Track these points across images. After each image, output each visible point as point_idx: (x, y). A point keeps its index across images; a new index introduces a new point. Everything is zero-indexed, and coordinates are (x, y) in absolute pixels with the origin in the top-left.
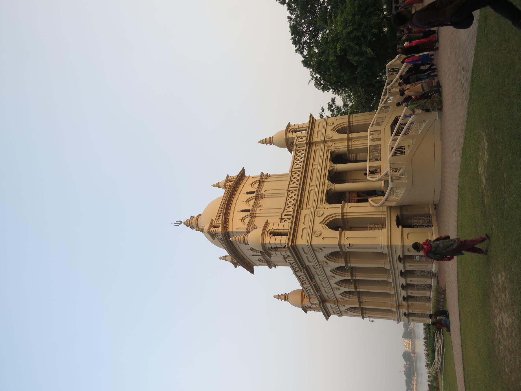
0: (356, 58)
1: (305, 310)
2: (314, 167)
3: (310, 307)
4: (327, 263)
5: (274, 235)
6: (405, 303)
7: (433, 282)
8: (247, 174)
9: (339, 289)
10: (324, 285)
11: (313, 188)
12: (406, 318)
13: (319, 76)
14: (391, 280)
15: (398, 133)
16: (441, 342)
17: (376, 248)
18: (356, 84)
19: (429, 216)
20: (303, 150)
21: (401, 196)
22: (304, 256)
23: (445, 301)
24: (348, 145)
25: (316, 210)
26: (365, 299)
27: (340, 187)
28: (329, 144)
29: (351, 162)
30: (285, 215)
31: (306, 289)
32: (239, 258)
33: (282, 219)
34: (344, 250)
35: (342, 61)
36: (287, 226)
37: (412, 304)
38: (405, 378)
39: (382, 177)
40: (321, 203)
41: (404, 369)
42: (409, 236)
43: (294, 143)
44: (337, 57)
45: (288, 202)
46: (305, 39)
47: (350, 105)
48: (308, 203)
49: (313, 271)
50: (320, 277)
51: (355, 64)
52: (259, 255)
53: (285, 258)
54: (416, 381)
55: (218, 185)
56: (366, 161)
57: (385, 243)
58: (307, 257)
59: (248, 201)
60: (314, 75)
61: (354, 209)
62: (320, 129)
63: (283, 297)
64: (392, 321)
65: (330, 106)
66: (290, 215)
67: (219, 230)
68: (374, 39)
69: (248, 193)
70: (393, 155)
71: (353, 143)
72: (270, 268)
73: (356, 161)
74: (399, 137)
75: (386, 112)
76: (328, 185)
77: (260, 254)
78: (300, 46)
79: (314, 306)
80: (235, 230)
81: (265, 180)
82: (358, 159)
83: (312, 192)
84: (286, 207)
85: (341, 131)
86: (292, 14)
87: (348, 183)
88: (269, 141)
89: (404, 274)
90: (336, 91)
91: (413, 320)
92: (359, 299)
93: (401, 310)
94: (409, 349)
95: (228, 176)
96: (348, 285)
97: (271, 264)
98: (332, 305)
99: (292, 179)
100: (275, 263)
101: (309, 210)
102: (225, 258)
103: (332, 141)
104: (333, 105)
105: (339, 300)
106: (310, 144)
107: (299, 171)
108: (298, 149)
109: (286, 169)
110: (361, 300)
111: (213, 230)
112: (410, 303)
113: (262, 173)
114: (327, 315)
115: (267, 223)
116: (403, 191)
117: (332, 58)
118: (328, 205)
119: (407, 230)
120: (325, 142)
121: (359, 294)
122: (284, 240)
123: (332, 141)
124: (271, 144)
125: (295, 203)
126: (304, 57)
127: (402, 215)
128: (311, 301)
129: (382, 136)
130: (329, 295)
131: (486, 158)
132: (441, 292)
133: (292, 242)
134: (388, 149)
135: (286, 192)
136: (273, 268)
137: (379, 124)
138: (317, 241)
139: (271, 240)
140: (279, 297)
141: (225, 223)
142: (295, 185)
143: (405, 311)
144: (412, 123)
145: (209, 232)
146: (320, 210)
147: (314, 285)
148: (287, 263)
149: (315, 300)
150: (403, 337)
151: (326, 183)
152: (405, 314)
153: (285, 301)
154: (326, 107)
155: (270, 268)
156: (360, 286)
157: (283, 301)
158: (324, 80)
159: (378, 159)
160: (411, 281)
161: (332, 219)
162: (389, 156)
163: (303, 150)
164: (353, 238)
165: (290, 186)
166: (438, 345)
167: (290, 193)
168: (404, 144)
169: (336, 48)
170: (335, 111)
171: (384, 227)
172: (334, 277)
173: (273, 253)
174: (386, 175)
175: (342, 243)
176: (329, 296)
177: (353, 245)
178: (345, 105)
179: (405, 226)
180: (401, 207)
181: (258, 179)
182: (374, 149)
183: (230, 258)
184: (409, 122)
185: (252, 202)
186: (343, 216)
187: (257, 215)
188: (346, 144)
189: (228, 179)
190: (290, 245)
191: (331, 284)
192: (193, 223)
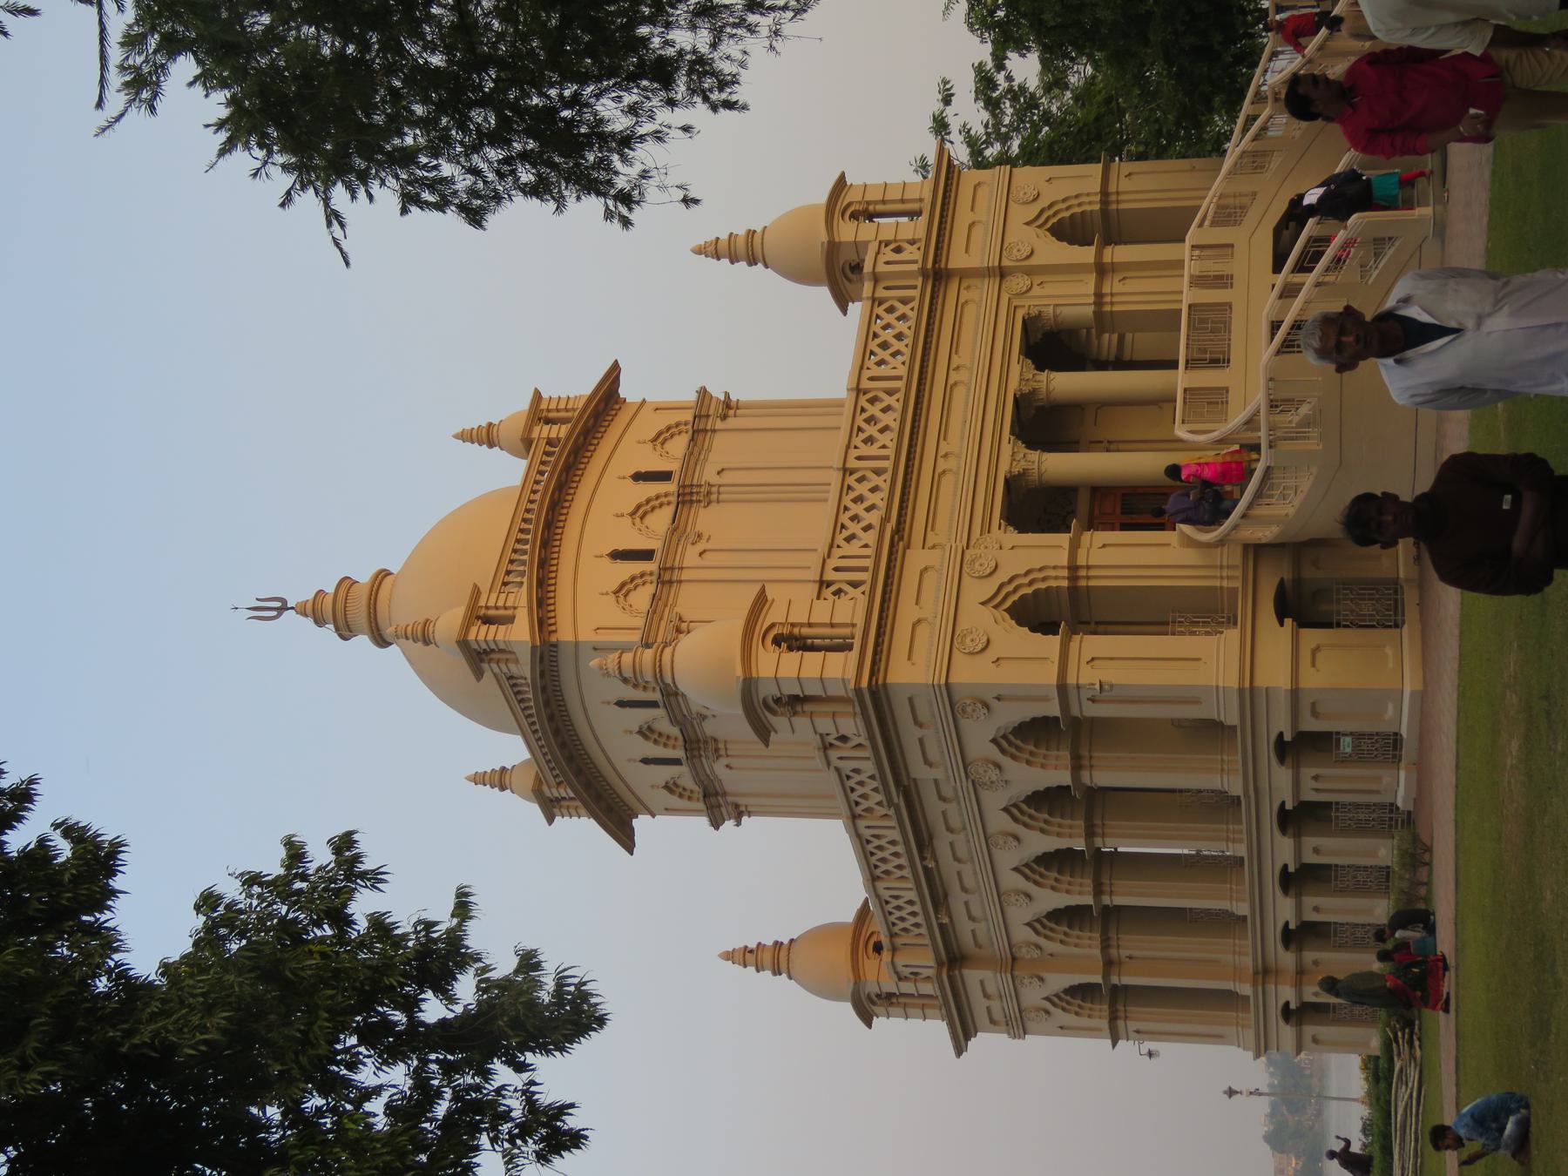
2: (954, 376)
3: (890, 995)
4: (998, 766)
5: (790, 649)
6: (1287, 959)
7: (1384, 852)
8: (628, 390)
10: (969, 882)
12: (1287, 1032)
15: (1303, 267)
16: (1413, 1074)
17: (1195, 701)
21: (1297, 502)
22: (909, 735)
23: (1427, 899)
24: (1099, 295)
25: (968, 554)
26: (1131, 945)
28: (1018, 283)
29: (1101, 365)
30: (837, 569)
33: (823, 584)
34: (1075, 712)
36: (850, 610)
37: (1316, 963)
39: (1236, 431)
40: (987, 528)
42: (1319, 656)
43: (867, 268)
45: (844, 518)
48: (930, 524)
49: (933, 808)
50: (959, 839)
52: (677, 762)
53: (826, 747)
55: (487, 437)
56: (1176, 367)
57: (1233, 683)
58: (921, 741)
59: (640, 512)
61: (1119, 556)
62: (982, 213)
63: (767, 957)
64: (1234, 1048)
65: (985, 83)
66: (865, 569)
67: (520, 633)
69: (638, 477)
70: (1278, 352)
73: (1120, 363)
74: (1310, 279)
77: (679, 753)
79: (906, 987)
80: (587, 635)
81: (719, 425)
82: (1127, 357)
83: (947, 482)
84: (840, 540)
85: (1069, 230)
87: (1088, 451)
91: (1315, 1040)
92: (1105, 946)
93: (1271, 988)
95: (537, 396)
96: (1066, 878)
97: (719, 806)
98: (988, 975)
99: (860, 421)
100: (741, 801)
101: (937, 551)
102: (499, 779)
103: (1030, 271)
104: (1000, 78)
105: (1023, 952)
106: (938, 276)
107: (890, 392)
108: (881, 293)
110: (1113, 952)
111: (481, 634)
112: (1309, 956)
113: (703, 393)
114: (962, 1033)
115: (761, 601)
116: (1306, 484)
118: (1013, 537)
119: (1311, 636)
120: (1002, 273)
121: (1110, 919)
122: (839, 669)
123: (1030, 271)
124: (752, 261)
125: (885, 520)
127: (1298, 581)
129: (1236, 267)
130: (981, 928)
132: (1417, 856)
133: (873, 673)
134: (1265, 329)
135: (835, 478)
136: (729, 825)
138: (968, 673)
139: (781, 668)
140: (747, 956)
141: (541, 603)
142: (872, 450)
143: (1287, 994)
144: (1347, 244)
145: (463, 644)
149: (924, 959)
152: (1287, 1013)
154: (965, 86)
155: (716, 824)
157: (768, 973)
160: (1316, 909)
161: (1029, 590)
162: (1265, 352)
164: (1112, 664)
165: (854, 453)
167: (851, 480)
171: (1232, 621)
172: (1017, 838)
173: (779, 722)
174: (1251, 423)
176: (982, 938)
177: (1112, 686)
179: (1304, 622)
181: (688, 416)
182: (1205, 321)
184: (1341, 237)
185: (661, 520)
186: (1073, 578)
187: (685, 575)
188: (1091, 289)
189: (540, 412)
190: (864, 684)
191: (1001, 884)
192: (353, 612)
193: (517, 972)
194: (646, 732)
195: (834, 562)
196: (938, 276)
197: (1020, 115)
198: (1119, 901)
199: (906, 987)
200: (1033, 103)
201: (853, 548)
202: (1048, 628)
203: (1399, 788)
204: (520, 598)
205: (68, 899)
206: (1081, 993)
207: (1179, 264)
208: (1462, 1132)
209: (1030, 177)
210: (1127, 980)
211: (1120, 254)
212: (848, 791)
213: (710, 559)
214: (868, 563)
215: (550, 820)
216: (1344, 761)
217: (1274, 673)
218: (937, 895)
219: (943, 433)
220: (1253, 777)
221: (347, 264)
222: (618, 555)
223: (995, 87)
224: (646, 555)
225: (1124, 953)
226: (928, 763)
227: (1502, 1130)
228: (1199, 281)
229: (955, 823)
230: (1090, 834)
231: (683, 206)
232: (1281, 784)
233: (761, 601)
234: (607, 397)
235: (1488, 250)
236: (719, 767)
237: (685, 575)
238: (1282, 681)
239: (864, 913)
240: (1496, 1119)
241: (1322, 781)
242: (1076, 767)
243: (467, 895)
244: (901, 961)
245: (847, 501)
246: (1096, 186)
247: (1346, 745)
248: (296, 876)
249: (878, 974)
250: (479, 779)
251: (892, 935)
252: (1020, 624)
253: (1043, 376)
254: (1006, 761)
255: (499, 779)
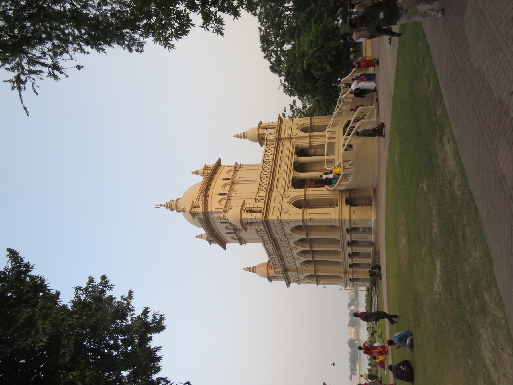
0: (319, 73)
1: (270, 279)
2: (282, 158)
3: (274, 277)
4: (291, 235)
5: (250, 213)
6: (350, 270)
7: (370, 250)
9: (299, 259)
10: (288, 256)
11: (281, 175)
12: (351, 283)
13: (287, 84)
14: (340, 250)
15: (349, 134)
16: (376, 295)
17: (330, 222)
18: (317, 92)
19: (369, 198)
20: (273, 144)
22: (274, 229)
23: (379, 261)
24: (310, 142)
26: (320, 267)
27: (302, 175)
28: (294, 140)
31: (272, 260)
32: (215, 237)
33: (256, 199)
35: (307, 74)
36: (261, 205)
38: (350, 364)
40: (288, 188)
41: (348, 356)
43: (265, 138)
44: (303, 70)
45: (261, 186)
46: (272, 48)
47: (308, 107)
50: (285, 248)
51: (317, 77)
52: (232, 233)
53: (258, 232)
54: (360, 366)
55: (196, 173)
57: (337, 218)
59: (224, 186)
60: (283, 82)
63: (251, 269)
65: (292, 107)
67: (200, 210)
68: (332, 59)
69: (224, 179)
71: (314, 140)
72: (241, 244)
73: (315, 155)
74: (350, 137)
75: (340, 116)
76: (293, 174)
77: (233, 232)
78: (268, 54)
79: (278, 275)
80: (213, 210)
83: (280, 179)
84: (260, 191)
85: (304, 130)
86: (262, 26)
88: (243, 136)
89: (351, 244)
90: (300, 96)
92: (315, 268)
93: (347, 275)
94: (353, 337)
95: (206, 165)
97: (241, 241)
98: (292, 273)
102: (201, 237)
103: (297, 138)
104: (294, 106)
105: (299, 269)
106: (279, 139)
107: (270, 162)
108: (268, 143)
109: (259, 161)
111: (194, 210)
112: (355, 269)
113: (236, 163)
114: (288, 283)
115: (244, 203)
117: (299, 71)
118: (293, 189)
119: (353, 208)
120: (291, 138)
121: (315, 263)
123: (297, 138)
124: (244, 138)
125: (268, 187)
126: (271, 63)
127: (350, 197)
128: (276, 271)
129: (336, 135)
130: (291, 264)
131: (398, 151)
132: (376, 253)
133: (265, 217)
134: (341, 145)
135: (259, 179)
136: (243, 244)
137: (334, 125)
138: (284, 217)
139: (248, 216)
140: (248, 269)
141: (205, 204)
143: (350, 276)
145: (190, 212)
146: (287, 193)
147: (279, 255)
148: (260, 237)
149: (280, 270)
150: (349, 325)
151: (292, 172)
152: (350, 280)
153: (253, 272)
154: (288, 108)
155: (241, 244)
156: (317, 256)
158: (291, 87)
159: (333, 154)
160: (355, 250)
162: (342, 150)
163: (273, 144)
164: (313, 214)
166: (374, 299)
167: (262, 179)
168: (353, 142)
169: (303, 63)
170: (296, 111)
171: (337, 205)
173: (248, 227)
175: (305, 218)
178: (304, 107)
179: (352, 205)
180: (350, 191)
183: (205, 237)
185: (228, 187)
187: (232, 198)
189: (206, 168)
191: (294, 256)
192: (173, 206)
193: (142, 315)
194: (226, 228)
195: (258, 195)
196: (279, 139)
197: (298, 113)
198: (317, 259)
199: (278, 275)
200: (300, 111)
201: (262, 192)
202: (300, 207)
203: (372, 238)
204: (201, 203)
205: (25, 298)
206: (311, 276)
207: (325, 136)
208: (395, 342)
209: (297, 120)
210: (319, 274)
211: (314, 134)
212: (263, 240)
213: (237, 195)
214: (265, 195)
215: (210, 244)
216: (361, 233)
217: (346, 216)
218: (282, 259)
219: (280, 170)
220: (342, 236)
221: (28, 115)
222: (220, 194)
223: (293, 108)
224: (225, 194)
225: (319, 269)
226: (278, 234)
227: (406, 341)
228: (329, 139)
229: (284, 245)
230: (310, 247)
231: (76, 69)
232: (348, 237)
233: (244, 203)
234: (218, 165)
235: (391, 123)
236: (241, 234)
237: (232, 198)
238: (347, 217)
239: (269, 261)
240: (404, 338)
241: (355, 237)
242: (307, 235)
243: (132, 292)
244: (276, 271)
245: (261, 183)
246: (309, 121)
247: (361, 230)
248: (90, 287)
249: (272, 273)
250: (197, 237)
251: (274, 266)
252: (295, 207)
253: (299, 158)
254: (293, 234)
255: (201, 237)
